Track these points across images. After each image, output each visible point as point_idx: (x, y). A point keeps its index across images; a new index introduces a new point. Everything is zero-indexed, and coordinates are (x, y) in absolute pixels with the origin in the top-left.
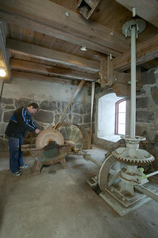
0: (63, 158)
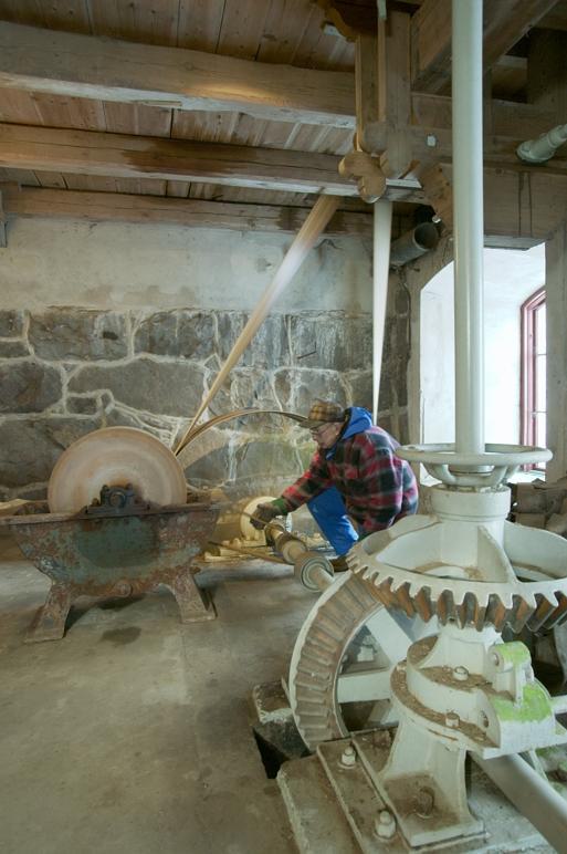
0: (179, 567)
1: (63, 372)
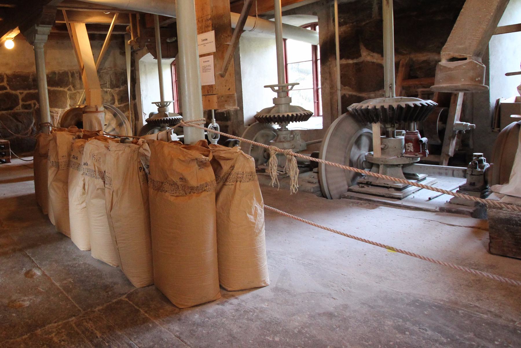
1: (19, 95)
